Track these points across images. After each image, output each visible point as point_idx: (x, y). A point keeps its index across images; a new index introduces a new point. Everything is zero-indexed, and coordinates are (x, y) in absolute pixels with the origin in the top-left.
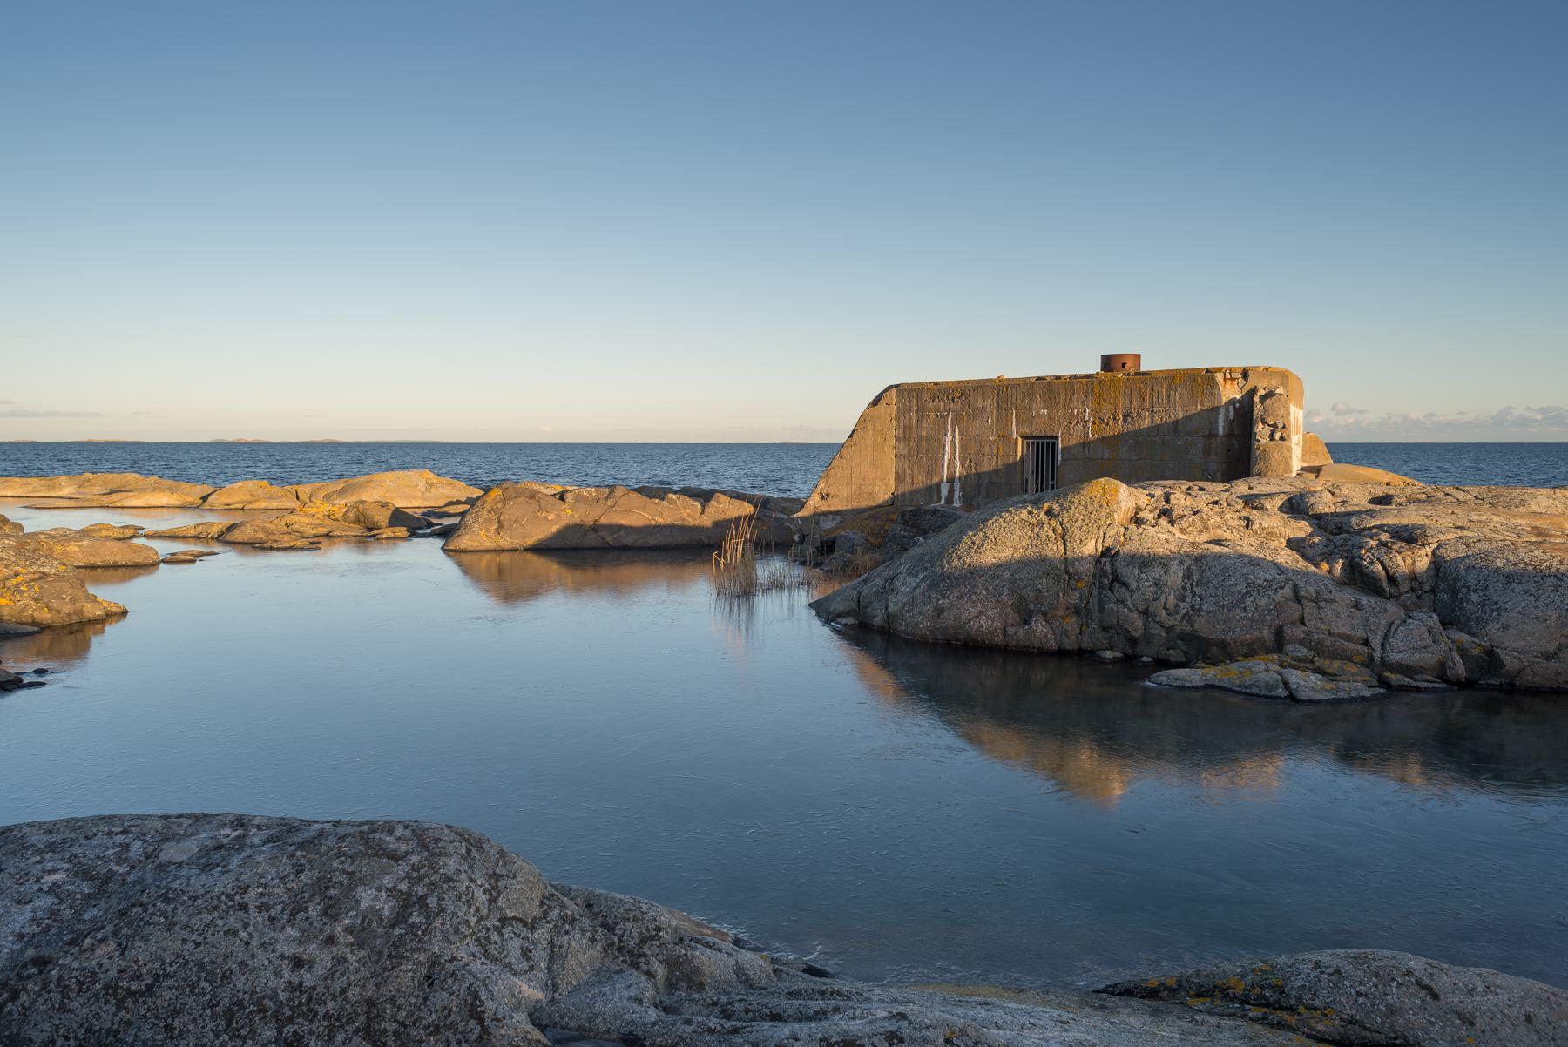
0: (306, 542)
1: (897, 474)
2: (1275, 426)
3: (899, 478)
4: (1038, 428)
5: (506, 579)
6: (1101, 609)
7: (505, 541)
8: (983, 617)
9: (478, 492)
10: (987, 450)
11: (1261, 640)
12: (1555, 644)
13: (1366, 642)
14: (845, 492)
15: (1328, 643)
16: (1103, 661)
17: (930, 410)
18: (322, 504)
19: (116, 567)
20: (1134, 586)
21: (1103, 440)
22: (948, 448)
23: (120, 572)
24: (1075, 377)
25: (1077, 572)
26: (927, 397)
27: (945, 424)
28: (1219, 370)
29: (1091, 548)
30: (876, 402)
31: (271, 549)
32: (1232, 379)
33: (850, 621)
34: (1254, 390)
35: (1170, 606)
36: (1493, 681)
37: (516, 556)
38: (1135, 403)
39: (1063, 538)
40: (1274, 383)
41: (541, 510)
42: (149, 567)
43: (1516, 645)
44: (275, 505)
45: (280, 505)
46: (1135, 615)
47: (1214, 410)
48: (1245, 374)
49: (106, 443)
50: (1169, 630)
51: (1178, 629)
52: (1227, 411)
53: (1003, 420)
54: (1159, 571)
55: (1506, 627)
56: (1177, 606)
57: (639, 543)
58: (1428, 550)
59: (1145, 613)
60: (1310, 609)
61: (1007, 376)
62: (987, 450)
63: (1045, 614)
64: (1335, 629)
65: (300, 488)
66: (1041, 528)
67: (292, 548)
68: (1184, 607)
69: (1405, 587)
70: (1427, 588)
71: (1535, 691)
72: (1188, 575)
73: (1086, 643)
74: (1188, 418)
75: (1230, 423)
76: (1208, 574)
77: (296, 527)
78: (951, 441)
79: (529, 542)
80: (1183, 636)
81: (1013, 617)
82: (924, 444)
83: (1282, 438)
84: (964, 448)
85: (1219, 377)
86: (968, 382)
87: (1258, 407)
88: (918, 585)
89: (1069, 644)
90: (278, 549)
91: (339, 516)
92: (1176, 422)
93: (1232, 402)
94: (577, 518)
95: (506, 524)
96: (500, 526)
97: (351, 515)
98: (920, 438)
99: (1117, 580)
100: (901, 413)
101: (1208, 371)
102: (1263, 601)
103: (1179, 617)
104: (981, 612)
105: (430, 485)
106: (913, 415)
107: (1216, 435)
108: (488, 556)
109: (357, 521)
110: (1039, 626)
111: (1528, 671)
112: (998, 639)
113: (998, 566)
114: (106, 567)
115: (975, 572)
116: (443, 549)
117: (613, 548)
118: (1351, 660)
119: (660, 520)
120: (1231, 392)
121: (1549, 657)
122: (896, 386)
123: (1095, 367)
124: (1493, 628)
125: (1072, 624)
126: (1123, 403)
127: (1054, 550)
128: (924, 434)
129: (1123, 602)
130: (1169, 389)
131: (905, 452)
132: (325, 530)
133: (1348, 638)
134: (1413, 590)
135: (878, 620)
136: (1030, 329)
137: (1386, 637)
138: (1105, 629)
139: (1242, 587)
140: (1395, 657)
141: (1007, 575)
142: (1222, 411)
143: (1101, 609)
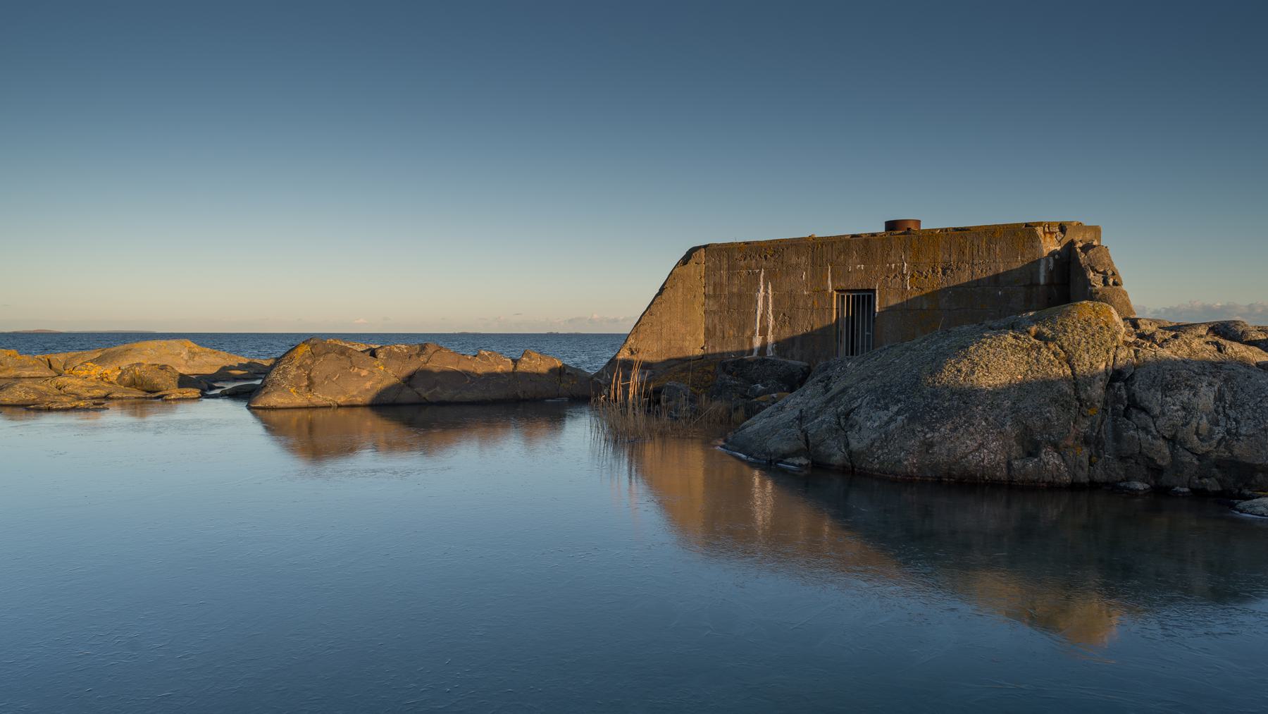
0: (90, 403)
1: (707, 329)
2: (1105, 273)
3: (709, 333)
4: (856, 282)
5: (313, 437)
6: (1118, 437)
8: (984, 449)
10: (801, 304)
14: (655, 347)
16: (1134, 493)
17: (742, 268)
18: (88, 374)
20: (1157, 411)
22: (760, 303)
25: (1089, 398)
26: (737, 255)
27: (758, 283)
28: (1039, 224)
31: (49, 410)
32: (1051, 233)
33: (804, 461)
34: (1071, 244)
38: (954, 257)
39: (1068, 362)
40: (1088, 236)
41: (353, 366)
44: (27, 373)
45: (32, 373)
46: (1161, 442)
47: (1036, 263)
48: (1063, 228)
50: (1201, 457)
51: (1214, 455)
56: (1211, 432)
57: (457, 398)
59: (1172, 441)
62: (801, 304)
63: (1056, 447)
65: (53, 357)
66: (1039, 352)
67: (75, 409)
68: (1219, 432)
72: (1220, 398)
73: (1100, 475)
75: (1050, 273)
76: (1241, 396)
77: (69, 389)
78: (764, 297)
80: (1219, 464)
81: (1016, 450)
82: (735, 300)
83: (1115, 284)
85: (1039, 230)
86: (781, 241)
88: (891, 420)
89: (1083, 477)
90: (57, 410)
91: (113, 378)
93: (1052, 254)
95: (317, 380)
96: (311, 386)
97: (127, 378)
98: (732, 294)
99: (1134, 404)
100: (710, 272)
101: (1027, 225)
103: (1214, 442)
104: (981, 445)
105: (193, 355)
106: (724, 273)
107: (1038, 284)
108: (299, 413)
109: (133, 384)
110: (1051, 459)
112: (1001, 474)
116: (249, 408)
117: (431, 404)
120: (1050, 245)
122: (705, 247)
125: (1084, 454)
126: (942, 256)
127: (1060, 371)
128: (735, 290)
129: (1146, 429)
130: (989, 242)
131: (715, 308)
132: (103, 393)
135: (838, 458)
138: (1122, 459)
141: (1007, 404)
143: (1118, 437)
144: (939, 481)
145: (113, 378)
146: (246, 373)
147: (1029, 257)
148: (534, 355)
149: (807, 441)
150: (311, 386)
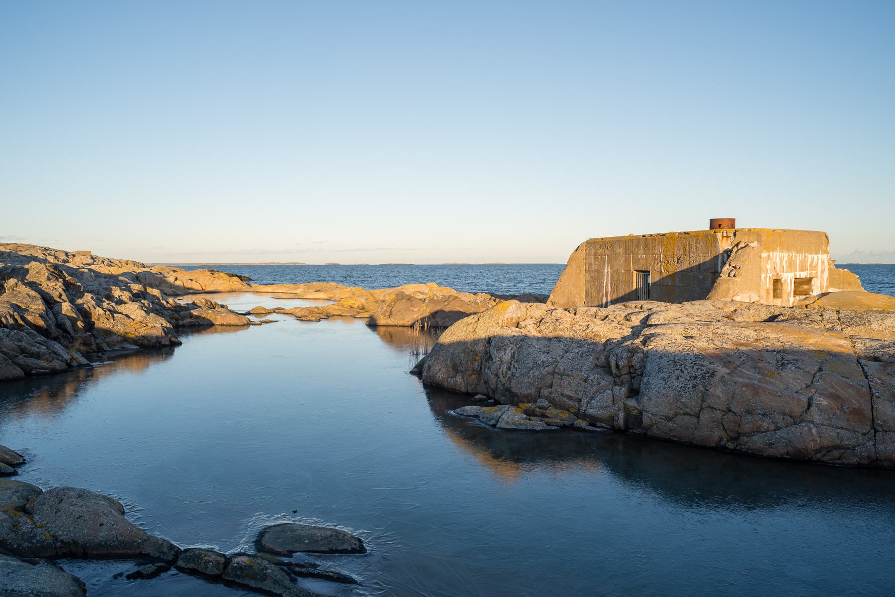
9: (705, 405)
12: (673, 412)
15: (557, 399)
19: (230, 325)
42: (250, 324)
43: (654, 410)
46: (493, 376)
47: (717, 257)
49: (381, 266)
55: (650, 399)
59: (496, 375)
60: (557, 380)
61: (635, 234)
69: (625, 371)
70: (639, 372)
72: (513, 357)
84: (611, 276)
87: (733, 254)
92: (700, 265)
102: (537, 373)
110: (459, 379)
114: (227, 325)
121: (669, 419)
123: (706, 227)
126: (677, 251)
133: (570, 398)
134: (630, 373)
136: (666, 206)
139: (531, 365)
140: (590, 411)
142: (720, 257)
145: (355, 306)
147: (714, 254)
150: (389, 316)
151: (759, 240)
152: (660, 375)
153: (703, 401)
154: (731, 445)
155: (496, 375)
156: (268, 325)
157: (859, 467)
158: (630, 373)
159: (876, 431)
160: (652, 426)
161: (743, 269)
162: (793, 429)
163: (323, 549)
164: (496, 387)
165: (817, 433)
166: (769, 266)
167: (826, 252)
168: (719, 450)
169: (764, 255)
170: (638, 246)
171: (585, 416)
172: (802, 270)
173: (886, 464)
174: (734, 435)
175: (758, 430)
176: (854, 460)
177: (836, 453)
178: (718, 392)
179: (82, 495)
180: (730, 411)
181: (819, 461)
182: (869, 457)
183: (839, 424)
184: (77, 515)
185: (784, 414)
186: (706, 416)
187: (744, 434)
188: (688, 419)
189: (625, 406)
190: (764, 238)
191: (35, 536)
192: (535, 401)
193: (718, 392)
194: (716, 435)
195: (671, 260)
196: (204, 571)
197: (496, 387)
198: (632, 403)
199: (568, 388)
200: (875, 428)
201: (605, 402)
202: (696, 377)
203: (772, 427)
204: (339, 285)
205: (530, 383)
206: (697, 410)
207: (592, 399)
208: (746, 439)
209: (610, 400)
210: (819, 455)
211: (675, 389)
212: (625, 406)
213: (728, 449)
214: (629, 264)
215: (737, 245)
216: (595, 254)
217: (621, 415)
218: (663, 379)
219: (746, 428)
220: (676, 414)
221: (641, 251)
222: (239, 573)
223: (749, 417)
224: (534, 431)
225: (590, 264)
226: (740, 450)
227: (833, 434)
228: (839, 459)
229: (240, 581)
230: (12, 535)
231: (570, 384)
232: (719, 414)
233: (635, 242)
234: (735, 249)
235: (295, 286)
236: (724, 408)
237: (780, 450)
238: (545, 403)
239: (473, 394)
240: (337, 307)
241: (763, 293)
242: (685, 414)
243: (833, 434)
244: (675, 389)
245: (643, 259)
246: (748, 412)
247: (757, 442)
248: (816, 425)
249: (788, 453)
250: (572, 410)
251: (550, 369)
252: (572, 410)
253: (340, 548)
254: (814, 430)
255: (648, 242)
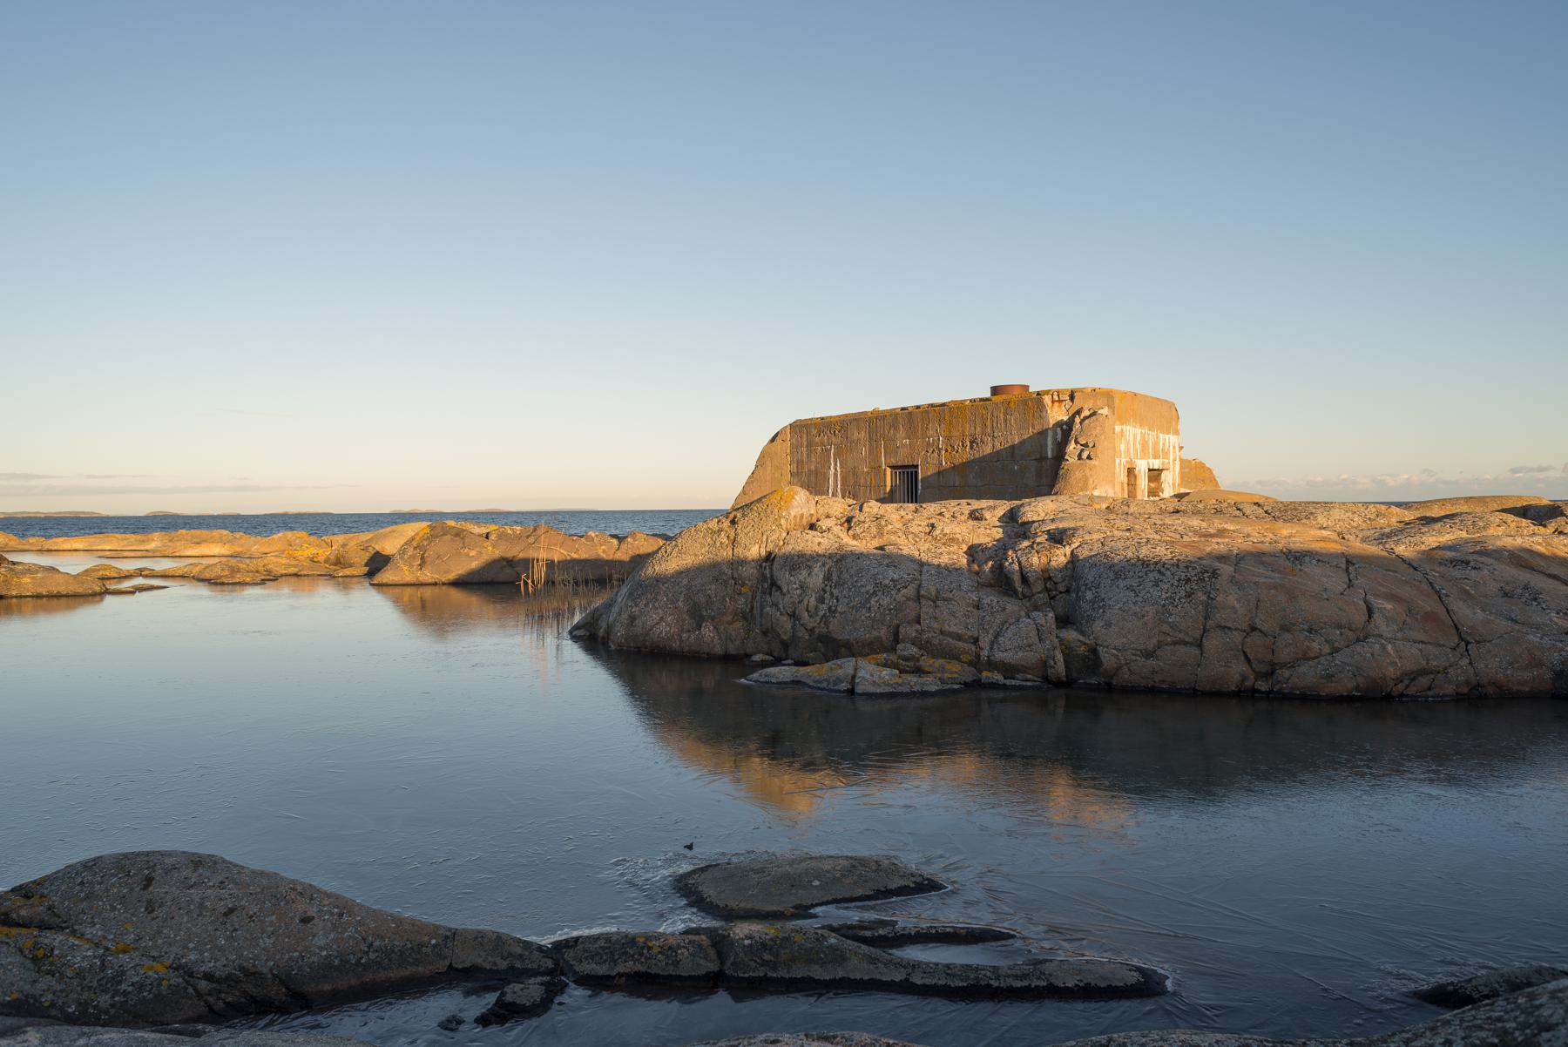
5: (427, 609)
7: (427, 575)
9: (1210, 623)
11: (879, 639)
12: (1154, 641)
13: (976, 641)
15: (936, 641)
19: (59, 596)
21: (955, 468)
23: (63, 600)
24: (932, 405)
28: (1047, 392)
29: (755, 551)
30: (773, 440)
35: (812, 609)
36: (1093, 681)
37: (436, 590)
41: (464, 547)
43: (1118, 642)
46: (785, 618)
47: (1043, 433)
50: (812, 631)
52: (1055, 433)
53: (874, 452)
54: (804, 573)
55: (1108, 625)
56: (817, 608)
58: (1068, 550)
59: (793, 615)
60: (926, 608)
63: (713, 619)
64: (946, 628)
68: (823, 608)
69: (1038, 587)
70: (1062, 588)
71: (1128, 690)
72: (828, 578)
74: (1023, 442)
76: (845, 576)
79: (451, 576)
83: (1089, 457)
84: (843, 478)
85: (1047, 399)
87: (1077, 426)
92: (1013, 447)
93: (1060, 424)
94: (497, 554)
99: (774, 585)
100: (795, 448)
102: (886, 601)
108: (409, 590)
110: (708, 631)
111: (1125, 669)
112: (676, 645)
113: (679, 573)
114: (51, 596)
115: (660, 580)
118: (959, 660)
119: (575, 556)
120: (1057, 414)
121: (1148, 654)
123: (988, 395)
124: (1098, 626)
130: (1006, 414)
133: (958, 637)
137: (997, 636)
139: (870, 588)
140: (999, 656)
141: (685, 582)
142: (1050, 433)
144: (638, 651)
145: (322, 559)
146: (354, 549)
147: (1038, 428)
148: (638, 536)
149: (1248, 660)
150: (421, 566)
151: (1111, 407)
152: (1122, 584)
153: (1206, 618)
154: (1263, 686)
155: (793, 615)
156: (145, 594)
157: (1459, 698)
158: (1047, 590)
159: (1467, 643)
160: (1119, 668)
161: (1099, 447)
162: (1358, 649)
163: (860, 892)
164: (794, 637)
165: (1393, 653)
166: (1122, 447)
167: (1177, 432)
168: (1244, 695)
169: (1118, 428)
170: (894, 426)
171: (992, 665)
172: (1155, 457)
173: (1490, 690)
174: (1263, 668)
175: (1306, 657)
176: (1450, 689)
177: (1424, 681)
178: (1232, 600)
179: (139, 874)
180: (1254, 629)
181: (1402, 695)
182: (1467, 683)
183: (1424, 637)
184: (221, 907)
185: (1340, 627)
186: (1213, 643)
187: (1284, 665)
188: (1182, 650)
189: (1061, 641)
190: (1117, 401)
191: (123, 973)
192: (894, 650)
193: (1231, 601)
194: (1236, 672)
195: (957, 443)
196: (671, 971)
197: (794, 637)
198: (1071, 635)
199: (954, 620)
200: (1465, 639)
201: (1025, 639)
202: (1188, 581)
203: (1327, 649)
204: (238, 535)
205: (874, 619)
206: (1197, 634)
207: (997, 636)
208: (1287, 673)
209: (1034, 633)
210: (1401, 687)
211: (1156, 603)
212: (1061, 641)
213: (1259, 691)
214: (878, 457)
215: (1078, 412)
216: (809, 444)
217: (1059, 657)
218: (1130, 588)
219: (1285, 654)
220: (1160, 645)
221: (901, 433)
222: (767, 957)
223: (1287, 636)
224: (924, 694)
225: (799, 463)
226: (1280, 692)
227: (1415, 651)
228: (1429, 689)
229: (783, 973)
230: (45, 982)
231: (953, 614)
232: (1237, 637)
233: (889, 420)
234: (1077, 420)
235: (139, 537)
236: (1245, 626)
237: (1345, 684)
238: (913, 650)
239: (748, 656)
240: (284, 561)
241: (1118, 488)
242: (1175, 643)
243: (1415, 651)
244: (1156, 603)
245: (903, 445)
246: (1285, 628)
247: (1306, 676)
248: (1389, 640)
249: (1357, 688)
250: (964, 658)
251: (910, 591)
252: (964, 658)
253: (893, 886)
254: (1389, 647)
255: (913, 419)
